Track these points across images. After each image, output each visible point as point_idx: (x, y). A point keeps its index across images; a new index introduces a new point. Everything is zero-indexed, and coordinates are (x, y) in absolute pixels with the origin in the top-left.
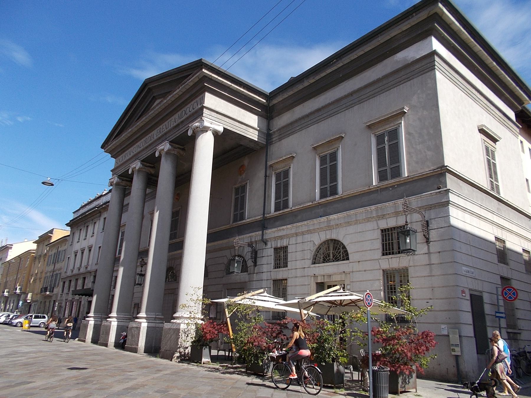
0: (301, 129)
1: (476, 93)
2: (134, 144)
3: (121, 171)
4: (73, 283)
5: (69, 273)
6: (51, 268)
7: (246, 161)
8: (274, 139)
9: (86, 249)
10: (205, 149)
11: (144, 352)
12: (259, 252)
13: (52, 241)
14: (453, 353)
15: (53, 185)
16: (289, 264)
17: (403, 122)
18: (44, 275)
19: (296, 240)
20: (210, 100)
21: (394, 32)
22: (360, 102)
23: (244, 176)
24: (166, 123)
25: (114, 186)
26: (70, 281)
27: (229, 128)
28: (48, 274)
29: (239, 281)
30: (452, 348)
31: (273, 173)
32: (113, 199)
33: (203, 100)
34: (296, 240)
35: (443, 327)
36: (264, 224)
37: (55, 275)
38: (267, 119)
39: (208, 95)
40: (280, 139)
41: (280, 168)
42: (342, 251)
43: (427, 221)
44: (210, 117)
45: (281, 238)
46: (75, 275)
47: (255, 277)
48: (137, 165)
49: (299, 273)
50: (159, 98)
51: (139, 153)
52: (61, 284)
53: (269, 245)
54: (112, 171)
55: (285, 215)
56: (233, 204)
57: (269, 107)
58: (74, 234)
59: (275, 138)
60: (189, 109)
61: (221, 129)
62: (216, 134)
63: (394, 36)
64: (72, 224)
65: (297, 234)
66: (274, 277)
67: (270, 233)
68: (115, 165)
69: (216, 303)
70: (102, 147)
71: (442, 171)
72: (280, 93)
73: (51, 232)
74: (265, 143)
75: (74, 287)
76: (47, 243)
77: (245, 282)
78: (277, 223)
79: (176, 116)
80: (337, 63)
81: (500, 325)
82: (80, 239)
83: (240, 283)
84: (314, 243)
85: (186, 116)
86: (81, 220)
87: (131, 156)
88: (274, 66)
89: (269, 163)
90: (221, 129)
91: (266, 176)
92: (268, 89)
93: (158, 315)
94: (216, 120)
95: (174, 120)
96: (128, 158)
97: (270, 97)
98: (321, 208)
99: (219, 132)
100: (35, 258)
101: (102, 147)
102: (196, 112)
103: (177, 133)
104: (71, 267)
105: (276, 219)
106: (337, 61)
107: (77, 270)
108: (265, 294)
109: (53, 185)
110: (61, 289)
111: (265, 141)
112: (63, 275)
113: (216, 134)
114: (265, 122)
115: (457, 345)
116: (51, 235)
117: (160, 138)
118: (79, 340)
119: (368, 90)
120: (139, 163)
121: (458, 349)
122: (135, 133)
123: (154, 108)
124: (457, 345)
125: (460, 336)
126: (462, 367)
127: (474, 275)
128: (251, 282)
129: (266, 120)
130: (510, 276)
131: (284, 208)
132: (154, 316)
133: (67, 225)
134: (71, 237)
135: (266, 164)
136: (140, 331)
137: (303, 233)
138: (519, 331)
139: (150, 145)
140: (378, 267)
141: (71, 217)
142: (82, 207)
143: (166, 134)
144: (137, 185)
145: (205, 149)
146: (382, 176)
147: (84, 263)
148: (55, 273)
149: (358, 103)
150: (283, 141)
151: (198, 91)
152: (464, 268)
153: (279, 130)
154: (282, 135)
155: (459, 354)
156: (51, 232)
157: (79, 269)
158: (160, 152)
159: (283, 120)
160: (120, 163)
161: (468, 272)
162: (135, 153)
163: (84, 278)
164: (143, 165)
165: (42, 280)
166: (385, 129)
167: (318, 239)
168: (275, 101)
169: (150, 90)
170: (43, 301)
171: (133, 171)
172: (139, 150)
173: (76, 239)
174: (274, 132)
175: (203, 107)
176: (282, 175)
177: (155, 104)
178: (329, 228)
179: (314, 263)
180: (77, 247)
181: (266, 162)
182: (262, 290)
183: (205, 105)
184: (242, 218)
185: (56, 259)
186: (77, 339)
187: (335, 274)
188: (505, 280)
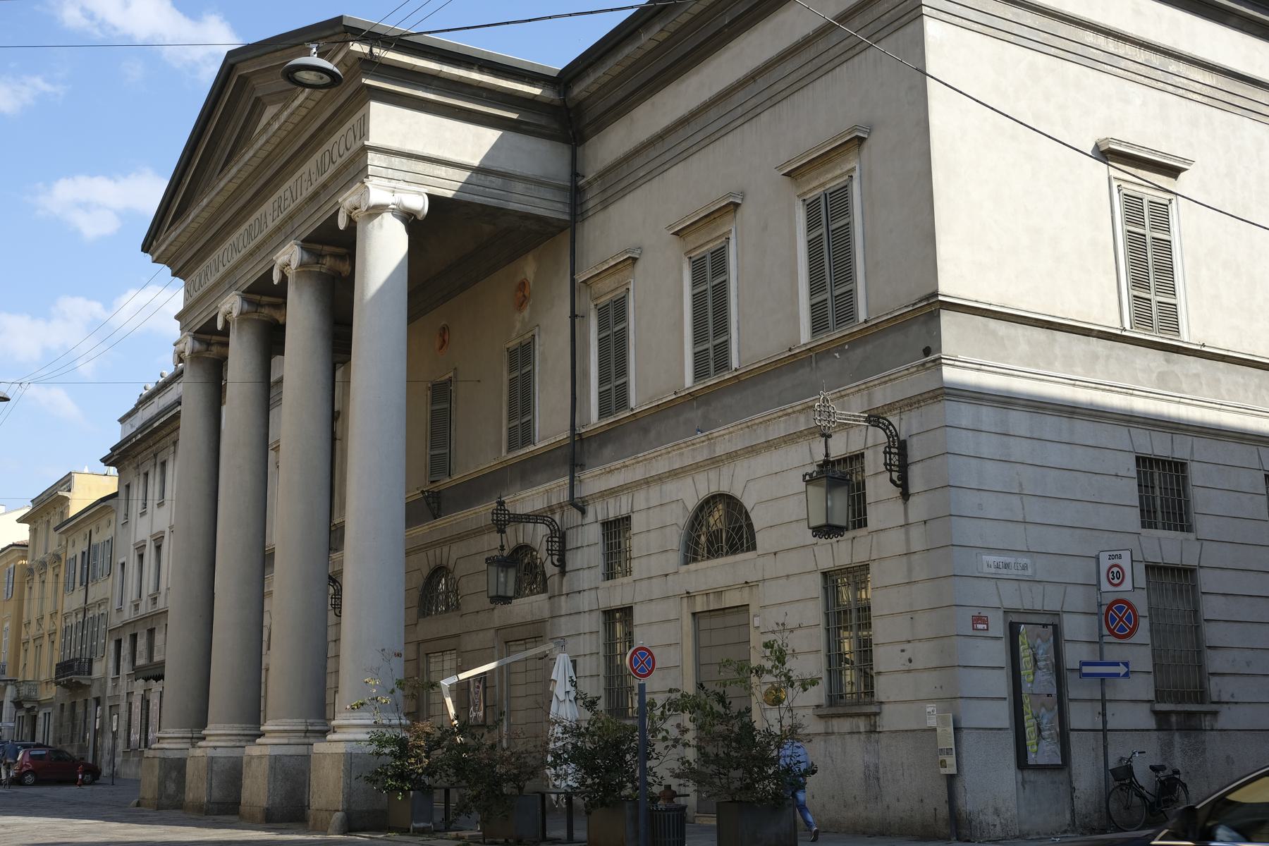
0: (650, 176)
1: (1101, 41)
2: (223, 240)
3: (200, 320)
4: (142, 643)
5: (128, 615)
6: (74, 601)
7: (529, 269)
8: (591, 204)
9: (148, 544)
12: (568, 532)
13: (73, 511)
14: (943, 771)
18: (59, 624)
19: (647, 500)
20: (387, 124)
22: (773, 101)
23: (526, 313)
24: (290, 183)
25: (188, 362)
26: (134, 637)
28: (72, 621)
29: (529, 618)
30: (941, 758)
31: (592, 306)
32: (190, 393)
33: (365, 121)
34: (647, 500)
35: (929, 710)
36: (576, 453)
37: (87, 621)
39: (378, 111)
40: (605, 204)
41: (607, 290)
44: (390, 173)
45: (614, 492)
46: (144, 619)
47: (564, 605)
48: (290, 255)
49: (657, 589)
50: (273, 103)
51: (236, 268)
52: (112, 646)
53: (590, 517)
54: (178, 317)
55: (625, 429)
56: (505, 398)
57: (564, 109)
58: (128, 487)
59: (592, 199)
60: (338, 144)
61: (419, 204)
62: (409, 218)
64: (119, 457)
65: (647, 482)
66: (604, 605)
67: (593, 481)
68: (186, 299)
70: (146, 248)
71: (932, 307)
73: (67, 482)
74: (567, 217)
75: (145, 654)
76: (56, 521)
77: (543, 621)
78: (608, 451)
79: (311, 165)
81: (1103, 695)
82: (149, 503)
83: (533, 623)
84: (685, 507)
85: (332, 169)
86: (144, 445)
87: (218, 275)
89: (580, 278)
90: (419, 204)
91: (573, 316)
92: (556, 59)
93: (312, 725)
94: (408, 177)
95: (306, 177)
96: (613, 102)
98: (698, 408)
99: (418, 212)
100: (30, 571)
101: (146, 248)
102: (351, 161)
103: (316, 217)
104: (131, 594)
105: (604, 437)
107: (150, 602)
109: (7, 399)
110: (111, 664)
111: (567, 210)
112: (115, 621)
113: (409, 218)
115: (948, 751)
116: (66, 494)
117: (278, 229)
119: (789, 66)
120: (297, 249)
121: (951, 760)
122: (221, 210)
123: (265, 129)
124: (948, 751)
125: (957, 729)
126: (960, 802)
127: (1029, 572)
128: (556, 620)
129: (565, 146)
130: (1190, 560)
131: (618, 409)
132: (303, 728)
133: (106, 461)
134: (122, 496)
135: (573, 281)
137: (660, 479)
138: (1214, 707)
139: (252, 254)
140: (811, 567)
141: (115, 435)
142: (145, 401)
143: (291, 217)
144: (240, 357)
146: (818, 324)
147: (148, 588)
148: (90, 614)
149: (769, 103)
150: (611, 208)
152: (992, 559)
153: (602, 175)
154: (610, 192)
155: (953, 771)
156: (67, 482)
157: (137, 606)
159: (614, 143)
160: (196, 295)
161: (1007, 566)
162: (228, 265)
163: (151, 632)
164: (250, 302)
165: (58, 639)
166: (823, 184)
167: (691, 492)
169: (244, 80)
170: (67, 703)
171: (226, 323)
172: (237, 257)
173: (136, 506)
174: (589, 183)
175: (365, 149)
176: (612, 312)
177: (264, 121)
178: (715, 462)
179: (687, 561)
180: (142, 530)
181: (573, 274)
183: (374, 139)
184: (527, 438)
185: (89, 567)
187: (730, 588)
188: (1174, 579)
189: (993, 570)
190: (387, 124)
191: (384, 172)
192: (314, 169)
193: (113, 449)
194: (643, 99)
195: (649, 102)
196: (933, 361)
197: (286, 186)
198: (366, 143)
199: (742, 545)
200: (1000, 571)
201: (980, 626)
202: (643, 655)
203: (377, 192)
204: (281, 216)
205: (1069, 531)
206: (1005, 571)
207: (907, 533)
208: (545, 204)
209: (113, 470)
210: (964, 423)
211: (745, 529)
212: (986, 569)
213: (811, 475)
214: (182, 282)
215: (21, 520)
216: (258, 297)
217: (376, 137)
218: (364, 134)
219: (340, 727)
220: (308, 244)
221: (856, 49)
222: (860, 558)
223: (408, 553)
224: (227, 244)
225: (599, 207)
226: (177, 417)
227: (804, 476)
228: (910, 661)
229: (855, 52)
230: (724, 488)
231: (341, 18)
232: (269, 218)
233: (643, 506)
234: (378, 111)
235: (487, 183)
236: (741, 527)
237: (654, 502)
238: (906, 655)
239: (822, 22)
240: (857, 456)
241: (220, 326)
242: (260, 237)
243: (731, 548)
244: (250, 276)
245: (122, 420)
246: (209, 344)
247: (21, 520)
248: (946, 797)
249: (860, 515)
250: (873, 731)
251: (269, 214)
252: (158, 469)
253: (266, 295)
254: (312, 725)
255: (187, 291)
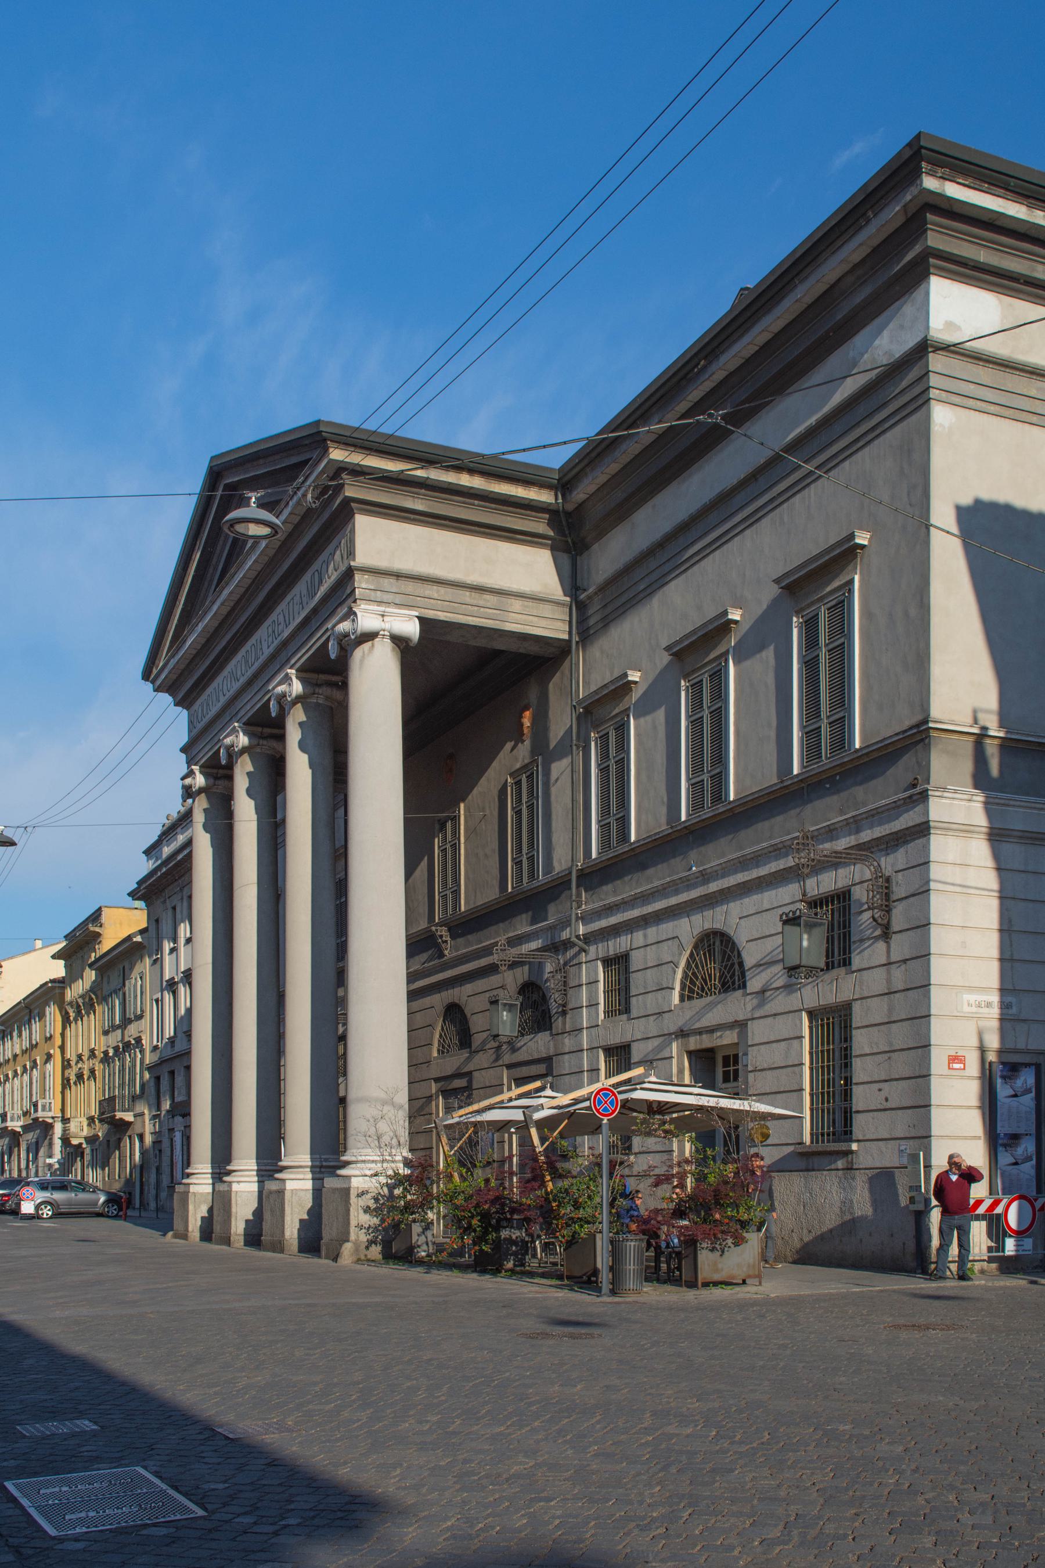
2: (222, 668)
10: (377, 693)
11: (299, 1252)
15: (13, 844)
16: (637, 1005)
17: (857, 578)
19: (645, 936)
21: (831, 269)
24: (283, 606)
26: (172, 1073)
27: (442, 616)
38: (567, 551)
42: (736, 961)
43: (888, 880)
47: (568, 1043)
54: (184, 750)
58: (157, 921)
61: (411, 629)
62: (399, 641)
63: (839, 280)
68: (190, 731)
69: (786, 1109)
73: (96, 917)
80: (710, 371)
88: (547, 395)
90: (411, 629)
92: (556, 459)
93: (326, 1160)
95: (297, 599)
96: (214, 710)
97: (564, 482)
101: (146, 676)
106: (710, 363)
108: (548, 1092)
109: (13, 844)
114: (565, 558)
116: (97, 929)
117: (273, 657)
133: (133, 895)
136: (283, 1199)
139: (250, 683)
145: (377, 693)
151: (333, 522)
152: (972, 998)
153: (602, 589)
156: (96, 917)
158: (279, 703)
159: (610, 555)
168: (579, 495)
172: (236, 686)
174: (589, 597)
182: (538, 1084)
186: (170, 1234)
189: (974, 1009)
190: (375, 541)
191: (373, 595)
192: (304, 592)
193: (140, 883)
194: (644, 501)
195: (650, 504)
196: (920, 793)
197: (278, 610)
198: (352, 563)
199: (734, 983)
200: (981, 1010)
201: (956, 1066)
203: (367, 618)
204: (276, 642)
205: (876, 1029)
207: (889, 973)
208: (544, 623)
209: (140, 904)
210: (950, 858)
211: (737, 967)
212: (966, 1009)
213: (787, 915)
214: (185, 712)
215: (54, 957)
216: (260, 729)
217: (363, 557)
218: (351, 553)
220: (303, 672)
221: (807, 481)
222: (845, 996)
223: (413, 995)
224: (225, 672)
225: (600, 625)
226: (190, 856)
227: (781, 916)
228: (887, 1100)
230: (718, 926)
231: (318, 423)
232: (265, 645)
233: (641, 943)
234: (363, 524)
235: (481, 603)
236: (733, 965)
238: (883, 1094)
239: (771, 453)
242: (257, 665)
243: (723, 986)
244: (249, 707)
245: (148, 852)
246: (216, 778)
247: (54, 957)
251: (264, 641)
252: (185, 904)
253: (268, 728)
254: (326, 1160)
255: (191, 723)
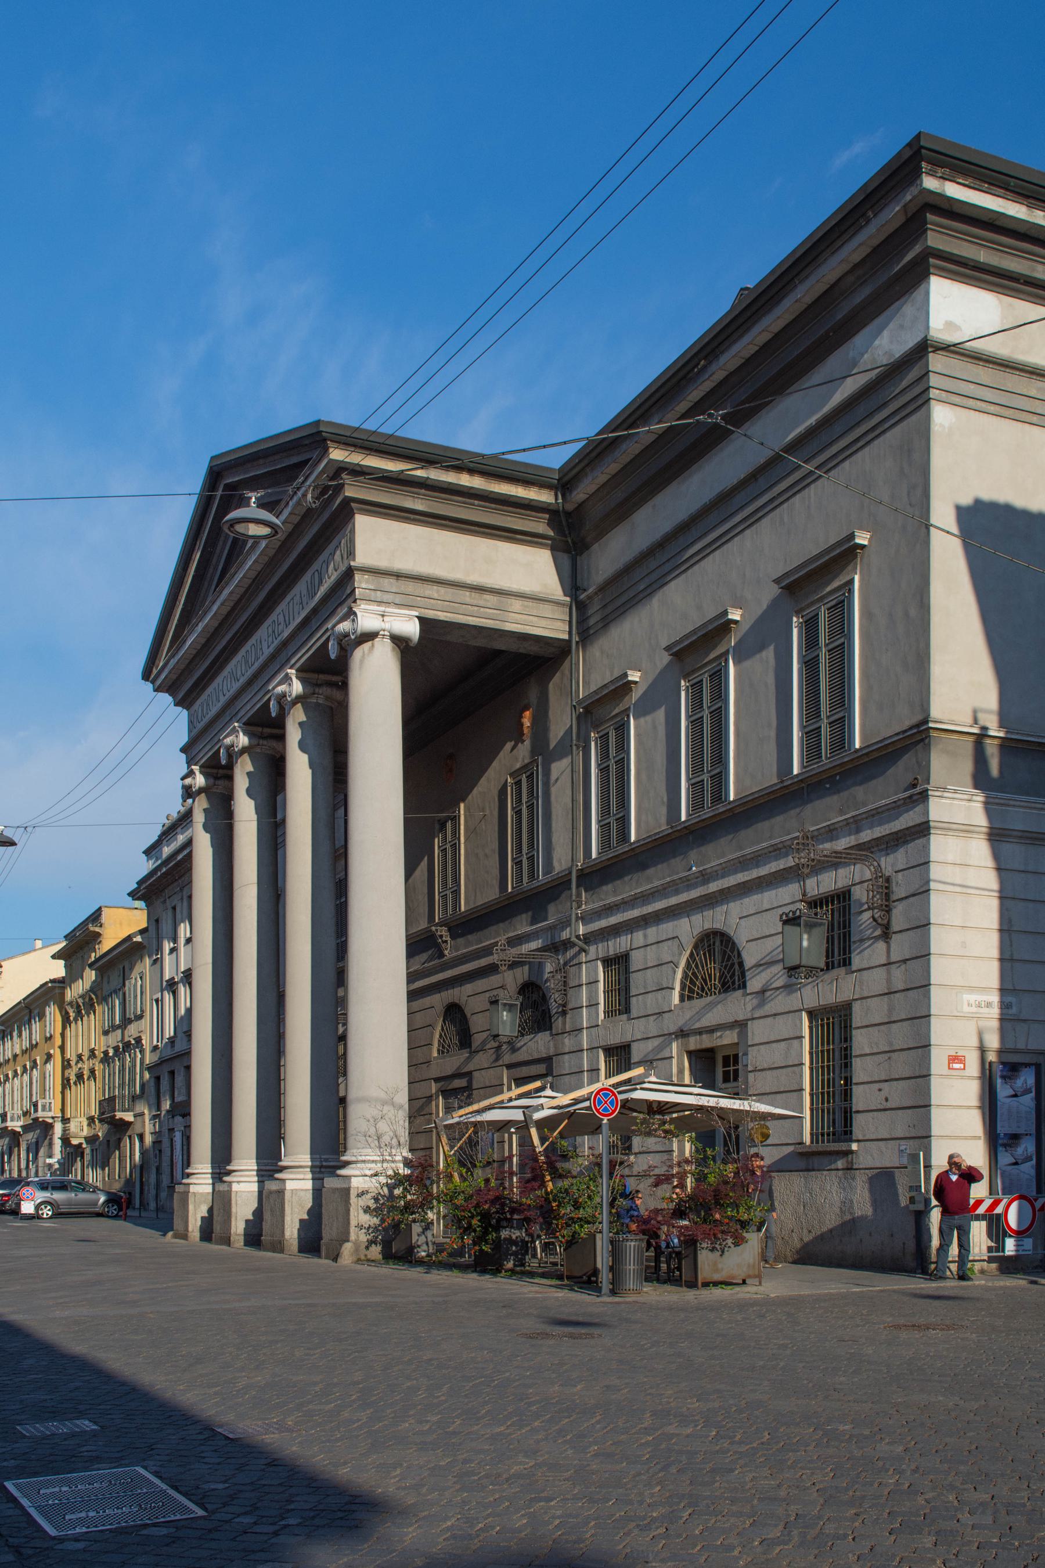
2: (221, 668)
10: (377, 693)
11: (300, 1251)
15: (13, 844)
17: (857, 578)
19: (645, 936)
21: (831, 269)
26: (172, 1073)
27: (442, 616)
38: (567, 551)
47: (568, 1043)
54: (184, 750)
58: (157, 921)
61: (411, 629)
62: (399, 641)
68: (190, 731)
72: (588, 470)
73: (96, 917)
88: (547, 395)
90: (411, 629)
92: (556, 459)
93: (326, 1160)
95: (297, 599)
96: (214, 710)
97: (564, 482)
101: (146, 676)
106: (710, 363)
108: (548, 1092)
109: (13, 844)
114: (565, 559)
116: (97, 929)
117: (273, 657)
118: (175, 1236)
119: (653, 564)
133: (133, 895)
136: (283, 1199)
139: (250, 683)
145: (377, 693)
151: (333, 522)
152: (973, 998)
154: (610, 609)
156: (96, 917)
159: (610, 555)
168: (579, 495)
172: (236, 686)
174: (589, 597)
182: (538, 1084)
186: (170, 1234)
189: (974, 1009)
190: (375, 540)
191: (373, 595)
192: (304, 592)
193: (140, 883)
194: (643, 501)
196: (920, 793)
197: (278, 610)
198: (352, 563)
199: (733, 983)
201: (956, 1066)
202: (606, 1095)
203: (367, 618)
204: (276, 642)
206: (986, 1010)
207: (889, 973)
208: (543, 623)
209: (140, 904)
210: (950, 858)
211: (737, 967)
212: (966, 1009)
213: (787, 915)
214: (185, 712)
215: (54, 957)
216: (260, 729)
217: (363, 557)
218: (351, 553)
219: (234, 1171)
220: (303, 672)
222: (844, 996)
223: (413, 995)
224: (226, 672)
225: (600, 625)
226: (189, 857)
227: (781, 916)
228: (887, 1100)
229: (860, 444)
230: (718, 926)
232: (265, 645)
233: (641, 943)
234: (363, 524)
235: (481, 603)
236: (733, 964)
237: (651, 940)
238: (884, 1094)
240: (844, 893)
241: (224, 762)
242: (257, 665)
243: (723, 986)
244: (249, 707)
246: (216, 778)
247: (54, 957)
248: (914, 1233)
249: (844, 954)
250: (849, 1168)
251: (264, 641)
254: (326, 1160)
255: (191, 722)
